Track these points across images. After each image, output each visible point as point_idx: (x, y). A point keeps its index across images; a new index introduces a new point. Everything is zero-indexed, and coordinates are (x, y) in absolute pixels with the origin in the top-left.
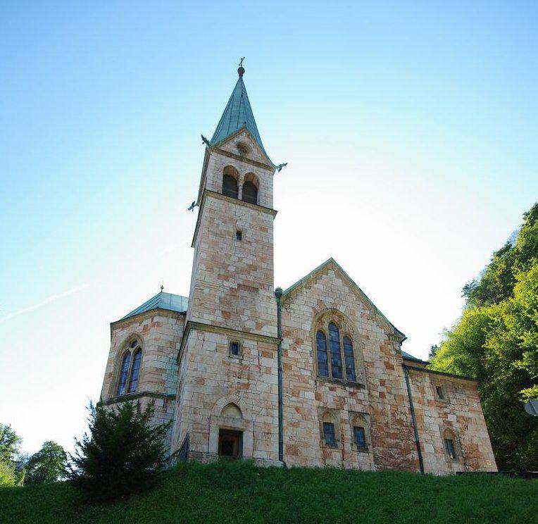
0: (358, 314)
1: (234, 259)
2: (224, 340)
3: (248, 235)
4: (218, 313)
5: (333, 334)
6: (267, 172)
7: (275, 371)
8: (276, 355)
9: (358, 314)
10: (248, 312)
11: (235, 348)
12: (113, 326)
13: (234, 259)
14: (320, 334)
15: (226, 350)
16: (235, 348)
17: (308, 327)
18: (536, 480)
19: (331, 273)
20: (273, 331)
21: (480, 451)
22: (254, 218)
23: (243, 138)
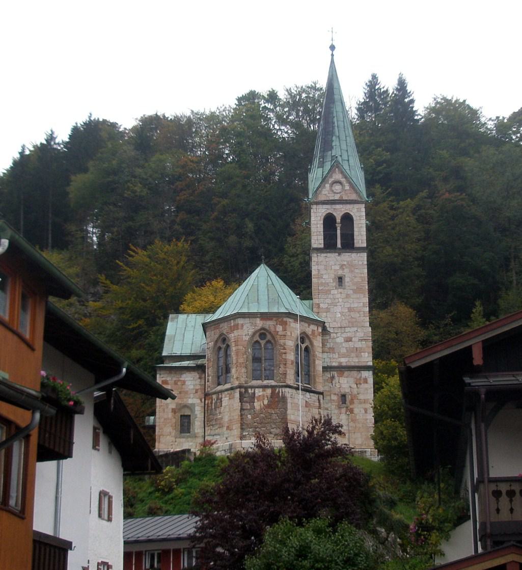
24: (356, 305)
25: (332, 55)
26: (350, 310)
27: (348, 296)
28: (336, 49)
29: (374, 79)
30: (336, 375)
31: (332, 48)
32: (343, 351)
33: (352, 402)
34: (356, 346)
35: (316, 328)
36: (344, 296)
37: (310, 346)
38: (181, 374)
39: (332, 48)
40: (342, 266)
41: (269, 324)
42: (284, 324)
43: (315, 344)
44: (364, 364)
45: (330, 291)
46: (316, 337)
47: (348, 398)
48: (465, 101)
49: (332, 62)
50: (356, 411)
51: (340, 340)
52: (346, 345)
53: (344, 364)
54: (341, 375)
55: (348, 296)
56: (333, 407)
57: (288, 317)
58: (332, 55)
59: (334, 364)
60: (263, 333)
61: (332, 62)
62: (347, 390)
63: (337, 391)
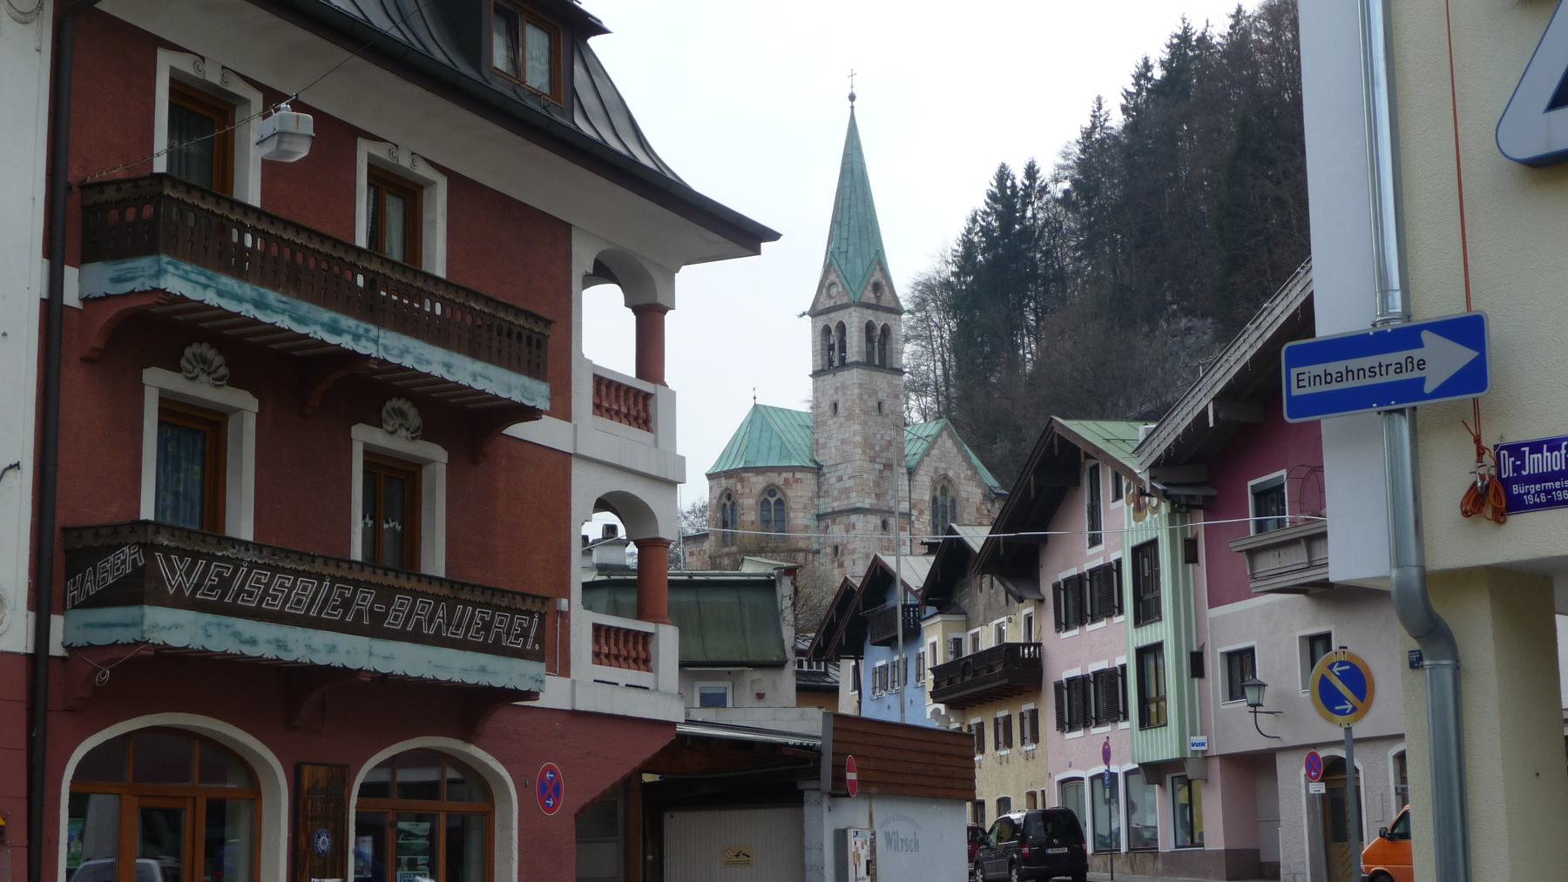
0: (962, 476)
1: (879, 437)
2: (875, 520)
3: (886, 406)
4: (873, 496)
5: (943, 497)
6: (893, 316)
7: (908, 543)
8: (908, 528)
9: (962, 476)
10: (890, 492)
11: (885, 525)
12: (1410, 652)
13: (879, 437)
14: (934, 500)
15: (880, 528)
16: (885, 525)
17: (927, 497)
18: (9, 881)
19: (1249, 655)
20: (904, 507)
21: (362, 580)
22: (889, 384)
23: (877, 276)
24: (847, 435)
25: (852, 107)
26: (843, 441)
27: (841, 426)
28: (848, 95)
29: (603, 31)
30: (830, 524)
31: (852, 98)
32: (836, 493)
33: (843, 554)
34: (846, 485)
35: (791, 474)
36: (837, 426)
37: (783, 498)
38: (703, 543)
39: (852, 98)
40: (836, 390)
41: (778, 480)
42: (742, 480)
43: (789, 494)
44: (852, 507)
45: (826, 422)
46: (791, 485)
47: (840, 549)
48: (1133, 76)
49: (852, 117)
50: (846, 563)
51: (833, 480)
52: (838, 486)
53: (836, 509)
54: (834, 522)
55: (841, 426)
56: (828, 561)
57: (745, 472)
58: (852, 107)
59: (829, 510)
60: (771, 490)
61: (852, 117)
62: (839, 540)
63: (830, 542)
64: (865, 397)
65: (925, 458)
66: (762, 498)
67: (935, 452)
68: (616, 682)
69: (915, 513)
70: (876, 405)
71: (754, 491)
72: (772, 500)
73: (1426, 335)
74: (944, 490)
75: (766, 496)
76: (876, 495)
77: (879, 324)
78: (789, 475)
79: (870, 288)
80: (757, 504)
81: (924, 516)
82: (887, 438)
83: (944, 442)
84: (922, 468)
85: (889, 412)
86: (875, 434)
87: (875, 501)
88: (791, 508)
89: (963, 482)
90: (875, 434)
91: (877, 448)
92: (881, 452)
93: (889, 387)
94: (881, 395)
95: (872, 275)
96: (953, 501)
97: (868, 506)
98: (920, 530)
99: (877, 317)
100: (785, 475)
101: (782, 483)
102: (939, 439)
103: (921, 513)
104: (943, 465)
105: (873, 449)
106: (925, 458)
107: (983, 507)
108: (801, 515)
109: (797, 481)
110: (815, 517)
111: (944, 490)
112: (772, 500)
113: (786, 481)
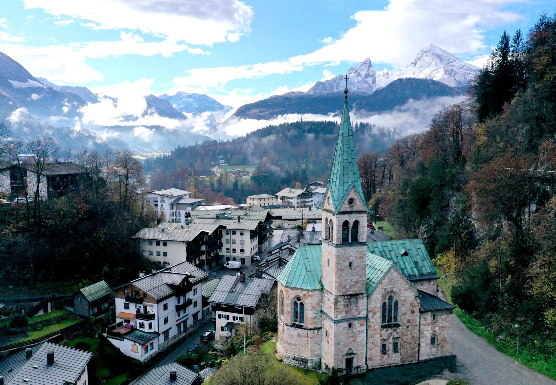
1: (349, 281)
2: (346, 324)
3: (354, 265)
4: (344, 312)
9: (402, 289)
11: (350, 325)
13: (349, 281)
20: (363, 314)
41: (301, 294)
64: (341, 262)
65: (379, 285)
66: (294, 301)
67: (386, 280)
68: (330, 265)
69: (370, 315)
70: (348, 264)
71: (290, 297)
72: (299, 302)
73: (123, 35)
74: (391, 298)
75: (296, 300)
76: (345, 312)
77: (351, 221)
78: (306, 292)
79: (347, 202)
80: (291, 303)
81: (376, 315)
82: (355, 280)
83: (392, 274)
84: (376, 291)
85: (356, 266)
86: (346, 280)
87: (344, 315)
88: (306, 308)
89: (403, 292)
90: (346, 280)
91: (348, 287)
92: (350, 288)
93: (357, 253)
94: (351, 259)
95: (348, 195)
96: (396, 302)
97: (340, 319)
98: (373, 322)
99: (350, 218)
100: (304, 292)
101: (303, 296)
102: (389, 273)
103: (375, 313)
104: (390, 286)
105: (345, 288)
106: (379, 285)
107: (415, 302)
108: (310, 312)
109: (309, 296)
110: (320, 312)
111: (391, 298)
112: (299, 302)
113: (305, 295)
